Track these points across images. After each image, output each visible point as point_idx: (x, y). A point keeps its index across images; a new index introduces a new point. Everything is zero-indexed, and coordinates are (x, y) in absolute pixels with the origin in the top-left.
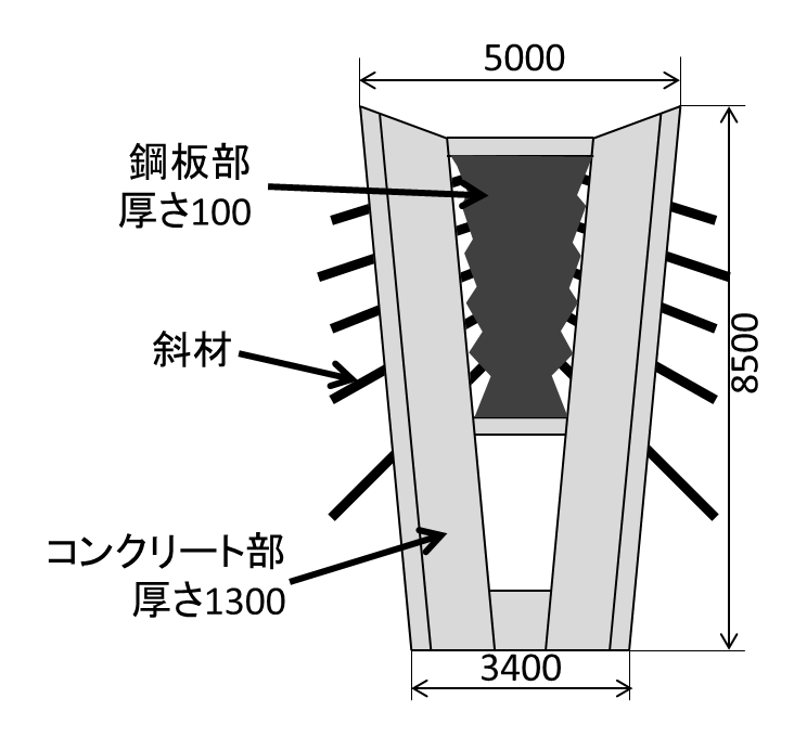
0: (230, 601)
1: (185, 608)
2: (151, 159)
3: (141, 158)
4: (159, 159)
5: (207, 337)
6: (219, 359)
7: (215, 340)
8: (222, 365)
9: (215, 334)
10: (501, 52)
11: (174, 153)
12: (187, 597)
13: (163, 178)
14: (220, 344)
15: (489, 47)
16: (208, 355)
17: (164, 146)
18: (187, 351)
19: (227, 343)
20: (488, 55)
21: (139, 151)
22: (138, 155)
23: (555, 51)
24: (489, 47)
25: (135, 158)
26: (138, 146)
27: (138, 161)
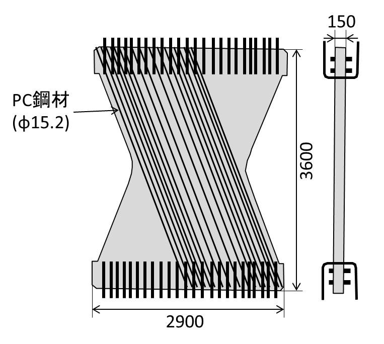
2: (42, 98)
3: (38, 98)
4: (46, 98)
5: (58, 94)
6: (63, 104)
7: (62, 95)
8: (65, 107)
9: (62, 92)
10: (345, 19)
11: (53, 95)
13: (48, 107)
14: (64, 97)
16: (58, 102)
17: (49, 92)
19: (67, 96)
21: (37, 94)
22: (37, 96)
23: (199, 318)
25: (35, 97)
26: (37, 92)
27: (36, 99)
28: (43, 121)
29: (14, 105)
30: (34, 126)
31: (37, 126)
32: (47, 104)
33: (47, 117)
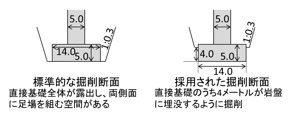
0: (251, 25)
1: (200, 84)
12: (200, 81)
15: (222, 53)
18: (77, 83)
20: (222, 56)
24: (222, 53)
28: (71, 18)
29: (93, 90)
30: (215, 74)
31: (217, 74)
32: (115, 95)
33: (219, 16)
